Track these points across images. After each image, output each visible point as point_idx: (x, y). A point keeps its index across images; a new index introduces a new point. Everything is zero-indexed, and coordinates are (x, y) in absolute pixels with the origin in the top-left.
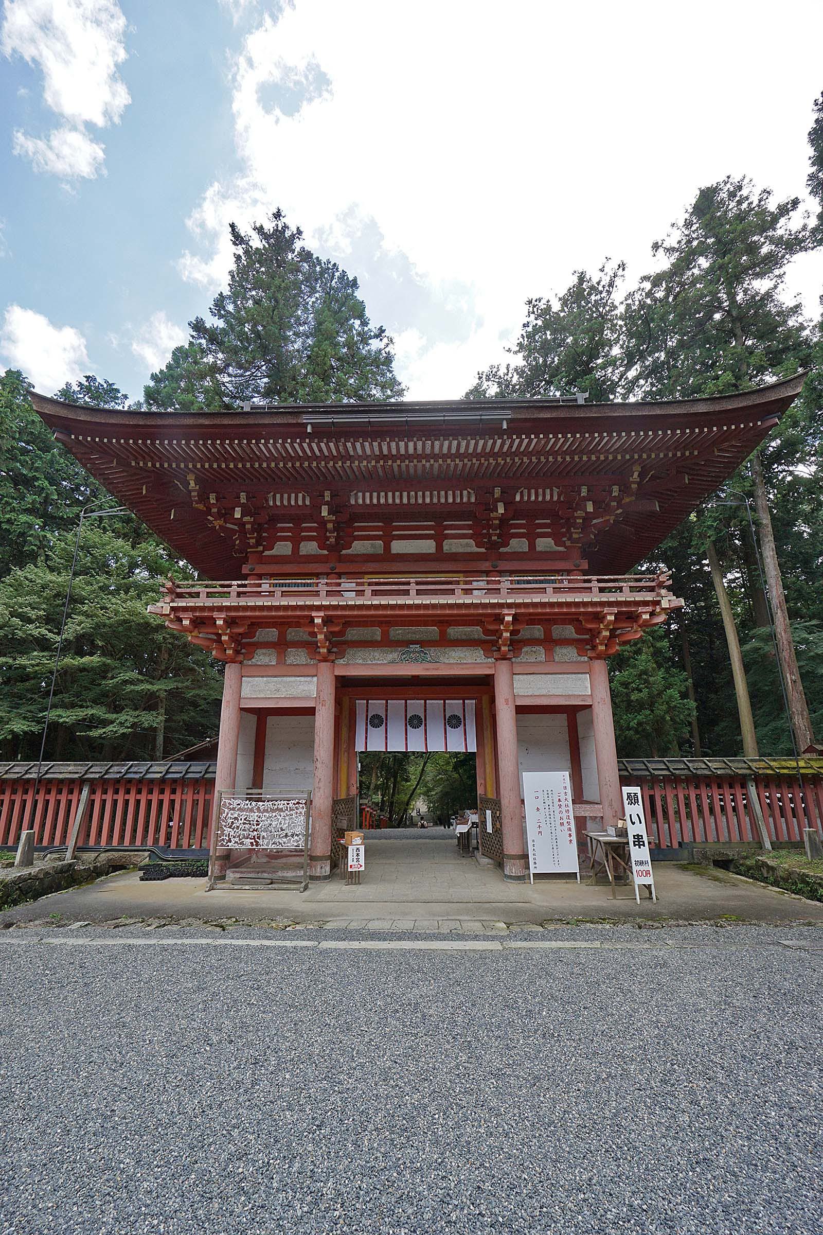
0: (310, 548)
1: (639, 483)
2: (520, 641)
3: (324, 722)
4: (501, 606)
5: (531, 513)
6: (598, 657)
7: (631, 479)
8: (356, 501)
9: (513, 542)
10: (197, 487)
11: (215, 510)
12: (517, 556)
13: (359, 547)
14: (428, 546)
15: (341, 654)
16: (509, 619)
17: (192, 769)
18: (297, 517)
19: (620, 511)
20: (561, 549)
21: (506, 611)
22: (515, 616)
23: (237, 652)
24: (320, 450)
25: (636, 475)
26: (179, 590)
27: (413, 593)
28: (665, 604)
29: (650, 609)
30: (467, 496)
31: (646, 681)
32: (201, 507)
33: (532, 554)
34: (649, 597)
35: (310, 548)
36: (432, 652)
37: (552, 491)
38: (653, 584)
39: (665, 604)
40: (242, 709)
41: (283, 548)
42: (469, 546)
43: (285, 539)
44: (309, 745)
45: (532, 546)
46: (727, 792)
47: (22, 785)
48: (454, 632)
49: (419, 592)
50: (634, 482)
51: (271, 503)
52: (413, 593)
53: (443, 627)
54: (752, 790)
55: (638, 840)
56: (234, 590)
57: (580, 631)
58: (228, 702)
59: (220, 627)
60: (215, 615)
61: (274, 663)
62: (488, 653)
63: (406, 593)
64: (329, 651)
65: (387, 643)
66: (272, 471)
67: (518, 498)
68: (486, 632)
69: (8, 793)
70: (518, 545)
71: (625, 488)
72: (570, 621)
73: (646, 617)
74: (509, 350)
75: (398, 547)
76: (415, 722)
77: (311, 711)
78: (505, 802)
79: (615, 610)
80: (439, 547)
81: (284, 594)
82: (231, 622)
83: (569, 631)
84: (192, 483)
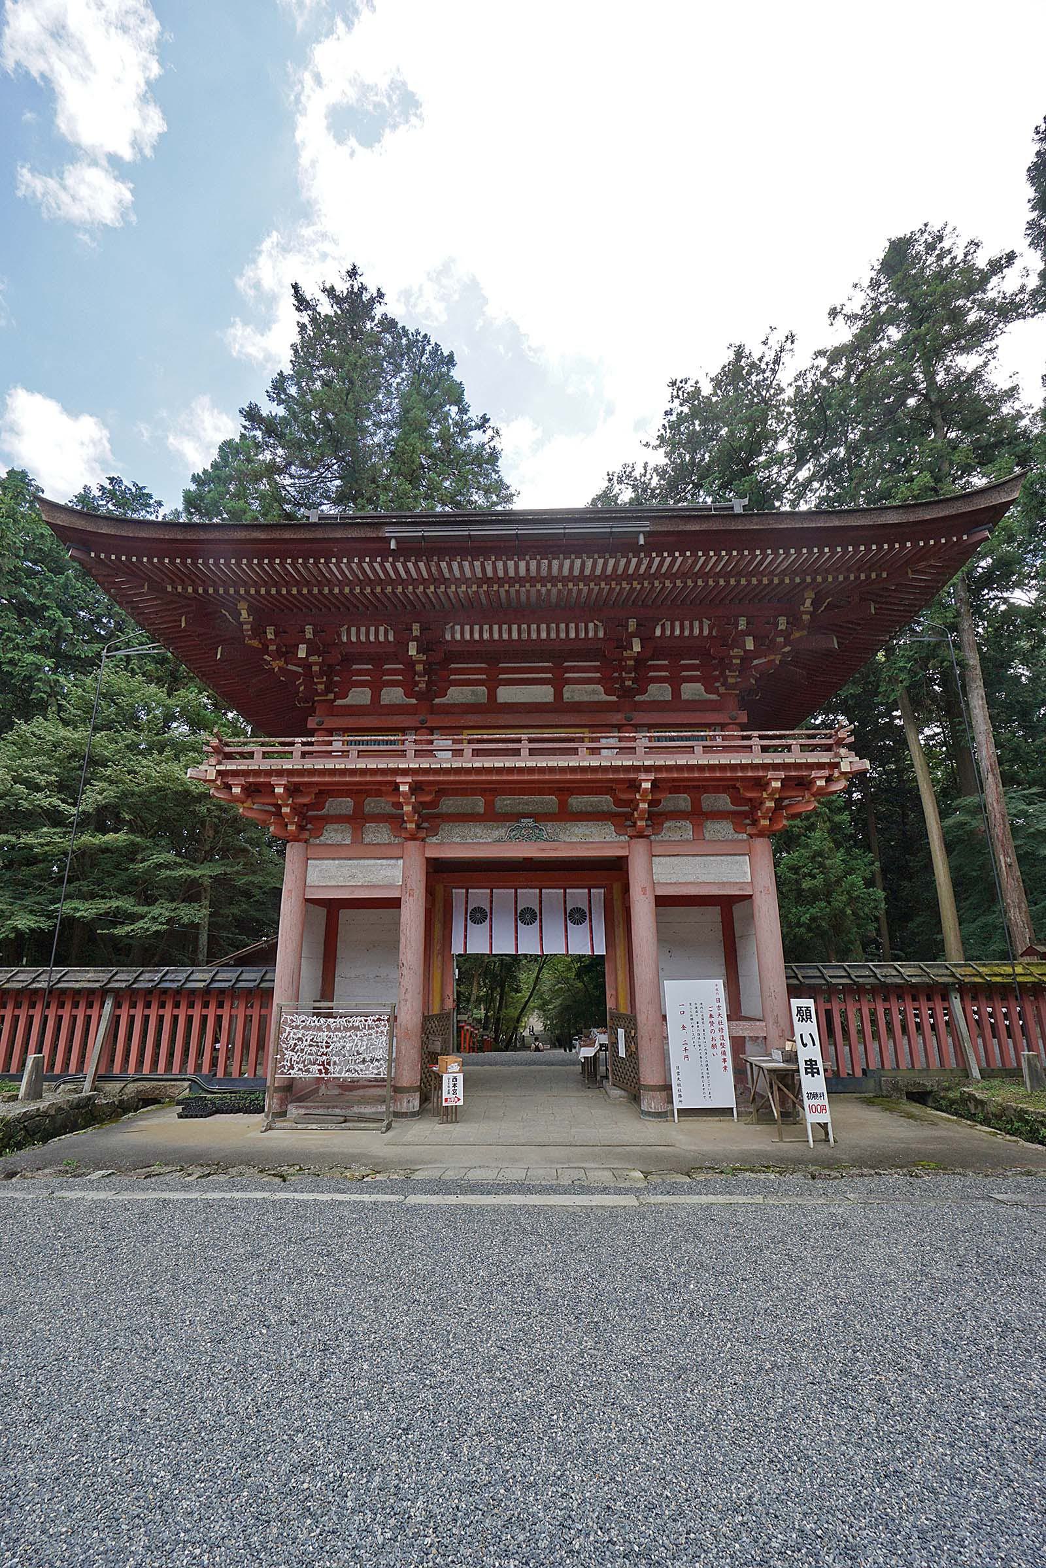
0: (393, 695)
1: (812, 614)
2: (661, 814)
3: (412, 916)
4: (637, 769)
5: (674, 651)
6: (761, 835)
7: (802, 608)
8: (453, 636)
9: (652, 688)
10: (251, 619)
11: (273, 648)
12: (657, 706)
13: (456, 695)
14: (543, 694)
15: (433, 831)
16: (647, 785)
17: (244, 976)
18: (378, 657)
19: (788, 649)
20: (713, 697)
21: (643, 776)
22: (654, 783)
23: (301, 828)
24: (407, 571)
25: (808, 603)
26: (227, 749)
27: (525, 753)
28: (845, 767)
29: (826, 773)
30: (594, 630)
31: (821, 865)
32: (255, 643)
33: (676, 703)
34: (825, 757)
35: (393, 695)
36: (549, 828)
37: (701, 623)
38: (830, 741)
39: (845, 767)
40: (307, 900)
41: (360, 696)
42: (596, 693)
43: (362, 684)
44: (392, 946)
45: (676, 693)
46: (924, 1005)
48: (577, 802)
49: (532, 752)
50: (806, 613)
51: (345, 639)
52: (525, 753)
53: (564, 796)
54: (956, 1003)
55: (811, 1067)
56: (298, 749)
57: (737, 801)
58: (290, 891)
59: (280, 796)
60: (274, 780)
61: (348, 842)
62: (620, 829)
63: (516, 753)
64: (418, 827)
65: (491, 816)
66: (346, 597)
67: (658, 633)
68: (618, 802)
70: (659, 692)
71: (794, 620)
72: (725, 789)
73: (821, 783)
74: (647, 445)
75: (506, 694)
76: (528, 916)
78: (641, 1018)
79: (782, 775)
80: (558, 694)
81: (360, 754)
82: (293, 790)
83: (723, 801)
84: (244, 614)
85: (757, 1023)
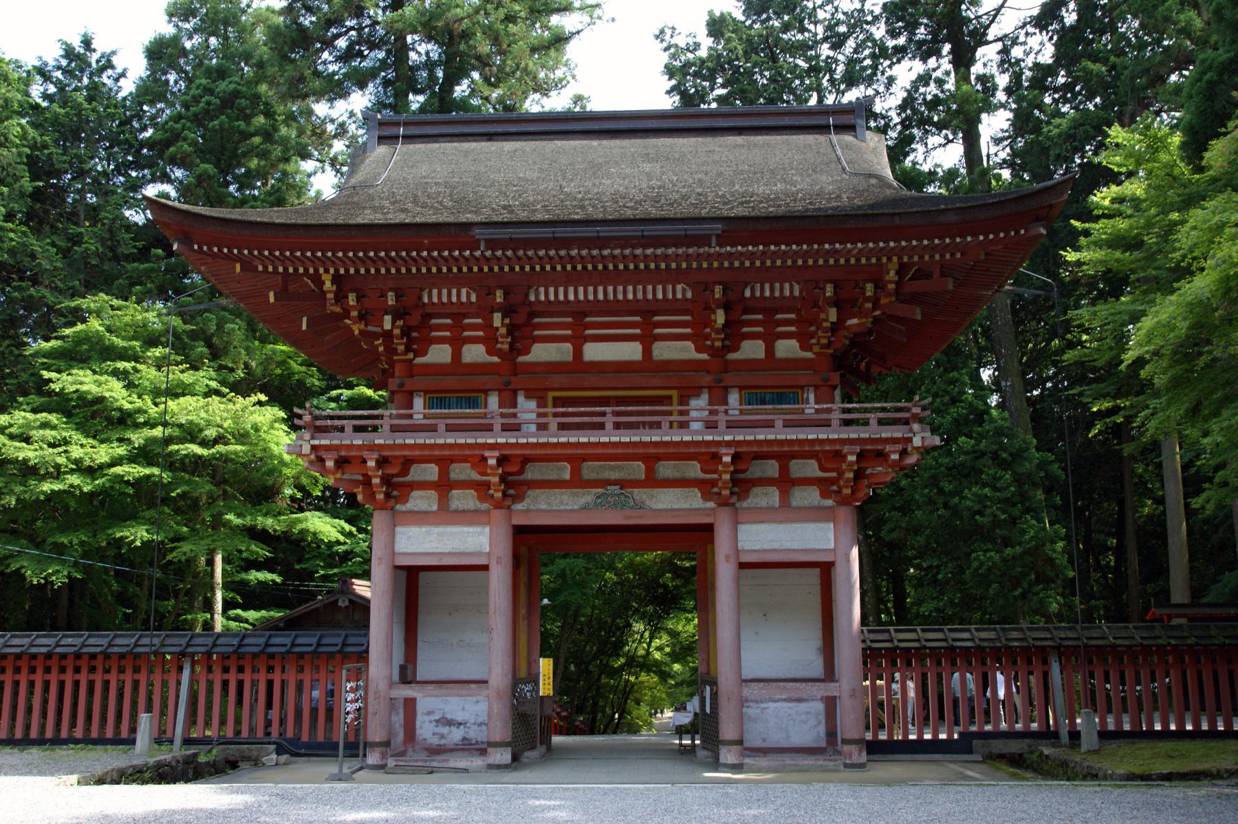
1: (897, 283)
3: (499, 581)
4: (719, 444)
5: (770, 309)
7: (887, 278)
8: (537, 296)
9: (746, 345)
10: (334, 288)
11: (354, 314)
12: (751, 365)
13: (542, 353)
14: (630, 351)
15: (519, 498)
16: (727, 459)
17: (324, 641)
18: (458, 314)
19: (877, 313)
20: (809, 355)
21: (724, 451)
23: (388, 496)
25: (892, 273)
26: (318, 423)
27: (609, 426)
28: (917, 442)
30: (681, 291)
32: (338, 309)
37: (791, 286)
38: (906, 415)
39: (917, 442)
40: (397, 567)
41: (440, 354)
43: (441, 340)
44: (482, 608)
47: (30, 661)
48: (666, 469)
49: (617, 426)
50: (891, 282)
51: (426, 300)
54: (1055, 669)
58: (380, 559)
59: (371, 469)
61: (435, 508)
62: (706, 496)
63: (601, 426)
64: (505, 495)
65: (577, 482)
69: (9, 672)
71: (879, 285)
73: (895, 457)
75: (595, 352)
77: (485, 568)
79: (858, 449)
80: (647, 352)
83: (811, 468)
85: (1137, 771)
